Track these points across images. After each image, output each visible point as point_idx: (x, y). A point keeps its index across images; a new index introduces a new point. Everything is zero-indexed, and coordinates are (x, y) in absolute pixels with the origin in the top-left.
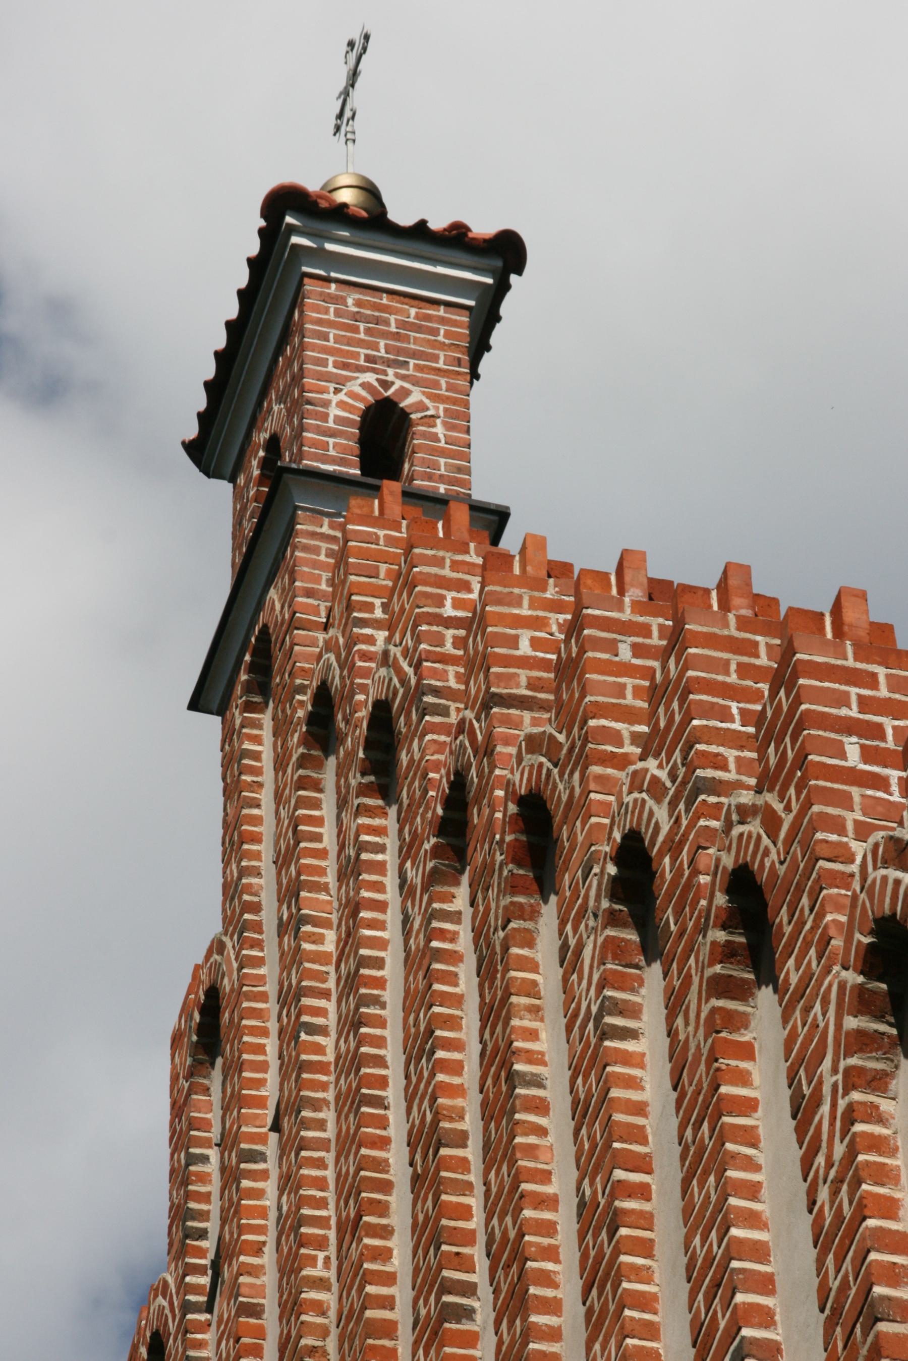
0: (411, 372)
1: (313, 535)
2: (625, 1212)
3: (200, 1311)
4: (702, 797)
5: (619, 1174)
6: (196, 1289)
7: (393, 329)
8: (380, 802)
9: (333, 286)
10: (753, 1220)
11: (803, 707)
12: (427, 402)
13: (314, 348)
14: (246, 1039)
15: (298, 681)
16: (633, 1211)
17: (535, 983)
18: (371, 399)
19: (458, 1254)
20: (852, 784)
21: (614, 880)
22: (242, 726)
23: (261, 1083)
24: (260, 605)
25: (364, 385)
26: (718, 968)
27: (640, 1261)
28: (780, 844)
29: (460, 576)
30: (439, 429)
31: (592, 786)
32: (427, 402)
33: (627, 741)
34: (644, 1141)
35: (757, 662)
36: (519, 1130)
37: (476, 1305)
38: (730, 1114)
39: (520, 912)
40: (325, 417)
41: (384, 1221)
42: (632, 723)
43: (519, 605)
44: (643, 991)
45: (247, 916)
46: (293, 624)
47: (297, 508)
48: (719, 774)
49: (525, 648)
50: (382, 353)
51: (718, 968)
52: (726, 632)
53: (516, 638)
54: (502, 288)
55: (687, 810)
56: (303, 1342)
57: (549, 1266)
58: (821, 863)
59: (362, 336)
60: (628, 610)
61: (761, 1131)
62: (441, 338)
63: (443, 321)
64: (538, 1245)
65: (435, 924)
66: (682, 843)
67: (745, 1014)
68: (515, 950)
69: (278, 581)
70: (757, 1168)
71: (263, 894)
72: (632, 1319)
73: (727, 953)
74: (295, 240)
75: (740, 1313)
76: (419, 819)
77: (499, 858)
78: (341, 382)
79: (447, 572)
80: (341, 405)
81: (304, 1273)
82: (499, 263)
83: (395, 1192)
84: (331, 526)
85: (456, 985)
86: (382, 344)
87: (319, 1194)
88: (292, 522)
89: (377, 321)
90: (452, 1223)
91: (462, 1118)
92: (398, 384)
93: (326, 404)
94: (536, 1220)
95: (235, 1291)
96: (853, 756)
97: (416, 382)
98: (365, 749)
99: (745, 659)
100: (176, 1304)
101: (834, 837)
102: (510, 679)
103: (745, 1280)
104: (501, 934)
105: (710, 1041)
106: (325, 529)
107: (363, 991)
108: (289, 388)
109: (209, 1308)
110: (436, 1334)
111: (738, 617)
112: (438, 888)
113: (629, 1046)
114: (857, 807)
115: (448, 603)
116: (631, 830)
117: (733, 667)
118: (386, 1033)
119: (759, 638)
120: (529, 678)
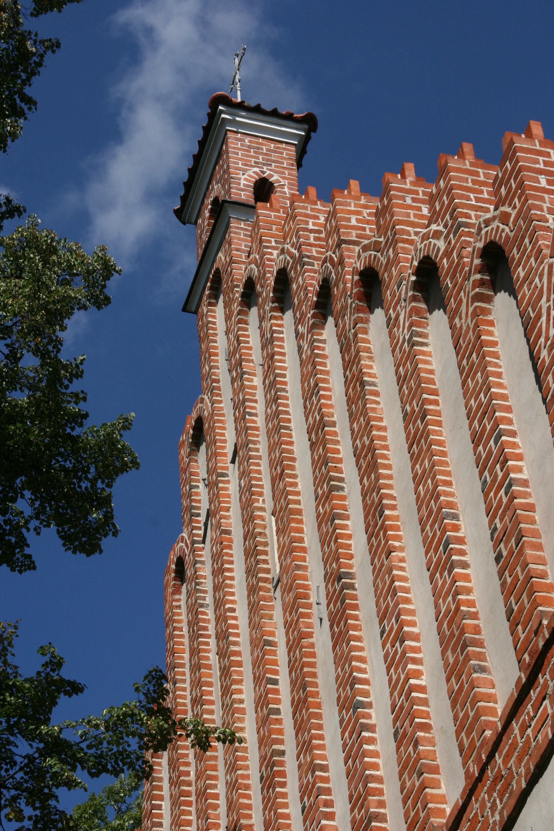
0: (273, 168)
1: (238, 228)
2: (429, 410)
3: (200, 543)
4: (462, 229)
5: (425, 396)
6: (198, 535)
7: (265, 151)
8: (280, 314)
9: (239, 135)
10: (500, 385)
11: (520, 164)
12: (280, 179)
13: (233, 158)
14: (217, 431)
15: (235, 283)
16: (432, 410)
17: (369, 348)
18: (257, 178)
19: (335, 467)
20: (544, 193)
21: (415, 282)
22: (207, 312)
23: (224, 447)
24: (214, 261)
25: (254, 172)
26: (477, 290)
27: (437, 428)
28: (511, 224)
29: (315, 213)
30: (286, 190)
31: (399, 251)
32: (280, 179)
33: (413, 234)
34: (434, 384)
35: (480, 179)
36: (368, 402)
37: (345, 485)
38: (486, 347)
39: (362, 320)
40: (239, 184)
41: (293, 472)
42: (414, 228)
43: (350, 206)
44: (429, 328)
45: (214, 384)
46: (231, 262)
47: (230, 217)
48: (468, 220)
49: (354, 222)
50: (261, 160)
51: (477, 290)
52: (465, 167)
53: (350, 219)
55: (454, 236)
56: (256, 530)
57: (385, 452)
58: (534, 222)
59: (252, 154)
60: (409, 185)
61: (500, 353)
62: (284, 156)
63: (285, 149)
64: (380, 444)
65: (315, 344)
66: (452, 251)
67: (489, 309)
68: (360, 335)
69: (223, 249)
70: (500, 367)
71: (220, 376)
72: (435, 449)
73: (481, 283)
74: (223, 116)
75: (498, 419)
76: (304, 307)
77: (349, 301)
78: (245, 171)
79: (309, 212)
80: (245, 179)
81: (254, 505)
82: (307, 127)
83: (297, 461)
84: (245, 225)
85: (326, 367)
86: (261, 157)
87: (258, 476)
88: (228, 223)
89: (258, 148)
90: (332, 455)
91: (333, 416)
92: (268, 172)
94: (379, 435)
95: (219, 525)
97: (275, 172)
98: (273, 292)
99: (474, 178)
100: (188, 542)
101: (539, 213)
102: (348, 234)
103: (499, 408)
104: (353, 331)
105: (474, 321)
106: (242, 226)
107: (278, 386)
108: (222, 177)
109: (204, 542)
110: (328, 497)
111: (470, 162)
112: (315, 331)
113: (424, 349)
114: (547, 202)
115: (311, 223)
116: (424, 257)
117: (470, 181)
118: (289, 402)
119: (479, 170)
120: (356, 234)
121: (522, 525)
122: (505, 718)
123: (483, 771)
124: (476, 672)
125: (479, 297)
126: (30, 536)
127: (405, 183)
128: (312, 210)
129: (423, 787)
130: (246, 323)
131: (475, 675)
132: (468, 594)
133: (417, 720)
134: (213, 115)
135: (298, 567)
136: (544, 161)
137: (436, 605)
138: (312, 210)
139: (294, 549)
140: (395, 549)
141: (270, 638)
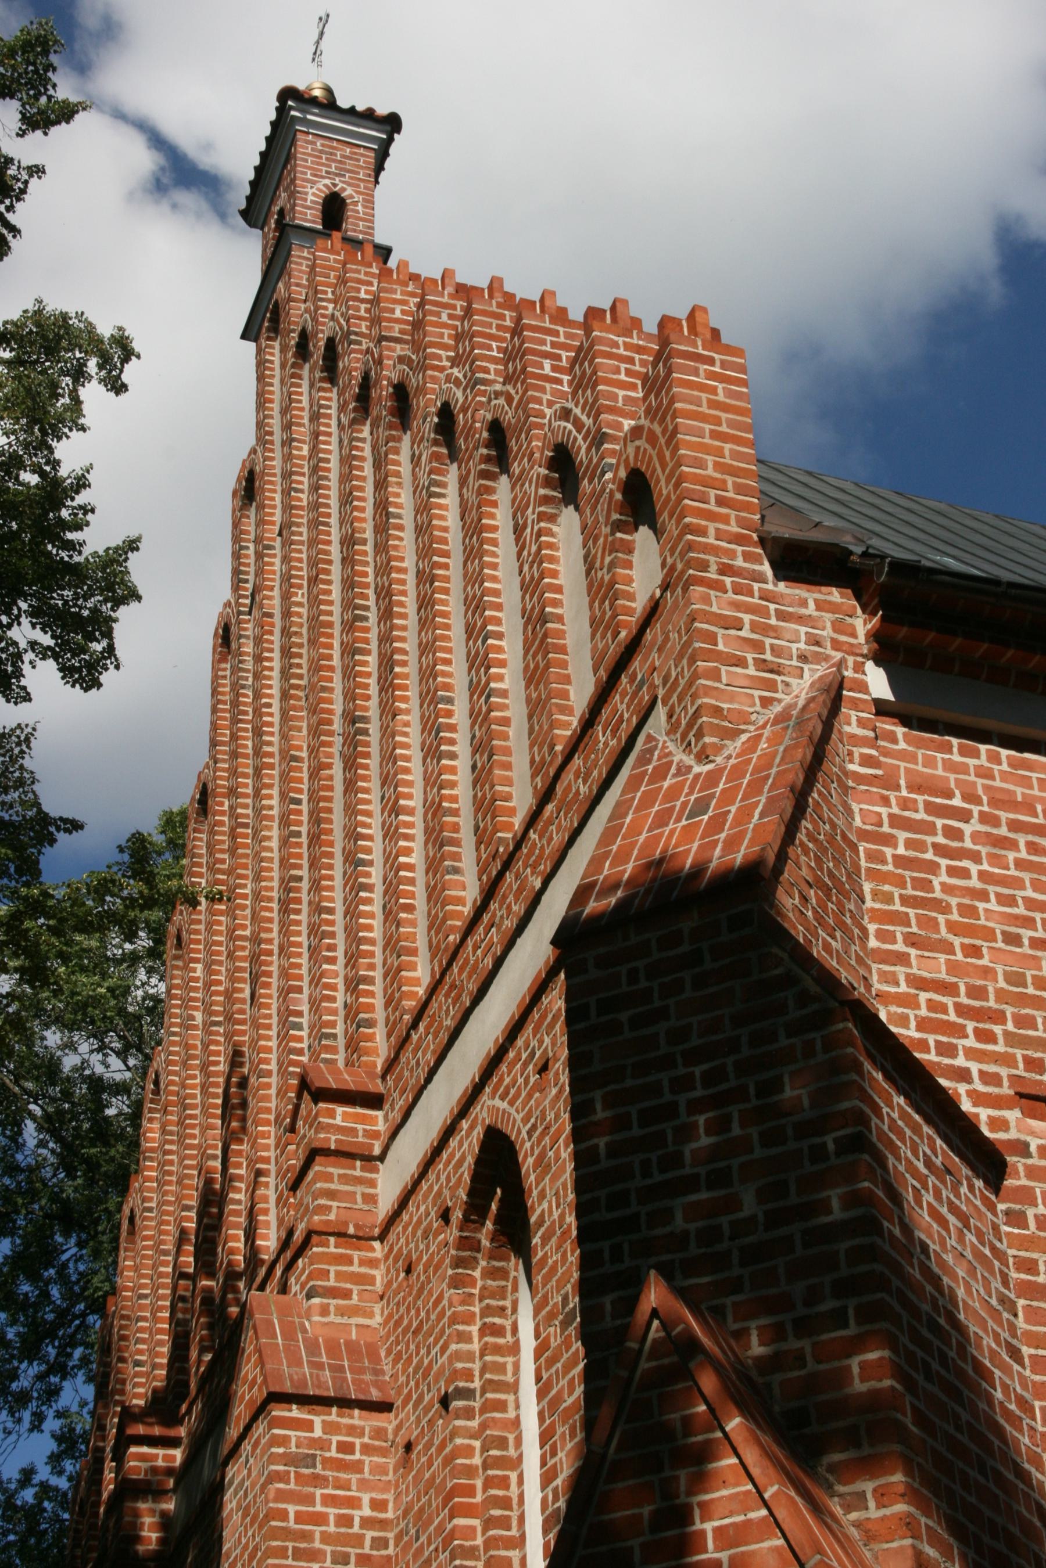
1: (300, 257)
5: (435, 558)
6: (244, 605)
21: (437, 425)
30: (360, 208)
34: (447, 544)
39: (393, 438)
40: (306, 200)
51: (483, 466)
54: (390, 140)
57: (403, 599)
63: (362, 155)
70: (497, 556)
73: (487, 459)
74: (293, 113)
78: (314, 183)
79: (362, 277)
80: (314, 194)
88: (290, 250)
89: (331, 154)
92: (341, 185)
93: (306, 193)
96: (547, 369)
97: (349, 184)
102: (390, 329)
109: (250, 613)
113: (442, 501)
121: (494, 742)
122: (612, 762)
123: (443, 974)
124: (449, 873)
125: (484, 475)
126: (26, 668)
127: (443, 296)
128: (366, 274)
129: (399, 970)
130: (300, 377)
131: (447, 877)
132: (452, 788)
133: (402, 901)
134: (282, 110)
135: (324, 689)
136: (552, 342)
137: (425, 792)
138: (366, 274)
139: (321, 668)
140: (401, 712)
141: (298, 753)
